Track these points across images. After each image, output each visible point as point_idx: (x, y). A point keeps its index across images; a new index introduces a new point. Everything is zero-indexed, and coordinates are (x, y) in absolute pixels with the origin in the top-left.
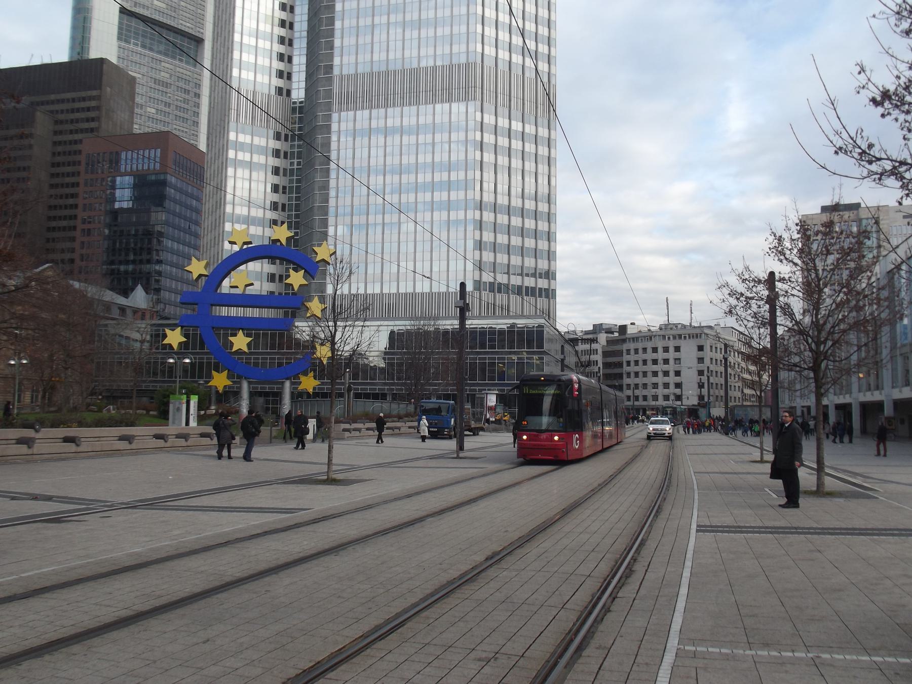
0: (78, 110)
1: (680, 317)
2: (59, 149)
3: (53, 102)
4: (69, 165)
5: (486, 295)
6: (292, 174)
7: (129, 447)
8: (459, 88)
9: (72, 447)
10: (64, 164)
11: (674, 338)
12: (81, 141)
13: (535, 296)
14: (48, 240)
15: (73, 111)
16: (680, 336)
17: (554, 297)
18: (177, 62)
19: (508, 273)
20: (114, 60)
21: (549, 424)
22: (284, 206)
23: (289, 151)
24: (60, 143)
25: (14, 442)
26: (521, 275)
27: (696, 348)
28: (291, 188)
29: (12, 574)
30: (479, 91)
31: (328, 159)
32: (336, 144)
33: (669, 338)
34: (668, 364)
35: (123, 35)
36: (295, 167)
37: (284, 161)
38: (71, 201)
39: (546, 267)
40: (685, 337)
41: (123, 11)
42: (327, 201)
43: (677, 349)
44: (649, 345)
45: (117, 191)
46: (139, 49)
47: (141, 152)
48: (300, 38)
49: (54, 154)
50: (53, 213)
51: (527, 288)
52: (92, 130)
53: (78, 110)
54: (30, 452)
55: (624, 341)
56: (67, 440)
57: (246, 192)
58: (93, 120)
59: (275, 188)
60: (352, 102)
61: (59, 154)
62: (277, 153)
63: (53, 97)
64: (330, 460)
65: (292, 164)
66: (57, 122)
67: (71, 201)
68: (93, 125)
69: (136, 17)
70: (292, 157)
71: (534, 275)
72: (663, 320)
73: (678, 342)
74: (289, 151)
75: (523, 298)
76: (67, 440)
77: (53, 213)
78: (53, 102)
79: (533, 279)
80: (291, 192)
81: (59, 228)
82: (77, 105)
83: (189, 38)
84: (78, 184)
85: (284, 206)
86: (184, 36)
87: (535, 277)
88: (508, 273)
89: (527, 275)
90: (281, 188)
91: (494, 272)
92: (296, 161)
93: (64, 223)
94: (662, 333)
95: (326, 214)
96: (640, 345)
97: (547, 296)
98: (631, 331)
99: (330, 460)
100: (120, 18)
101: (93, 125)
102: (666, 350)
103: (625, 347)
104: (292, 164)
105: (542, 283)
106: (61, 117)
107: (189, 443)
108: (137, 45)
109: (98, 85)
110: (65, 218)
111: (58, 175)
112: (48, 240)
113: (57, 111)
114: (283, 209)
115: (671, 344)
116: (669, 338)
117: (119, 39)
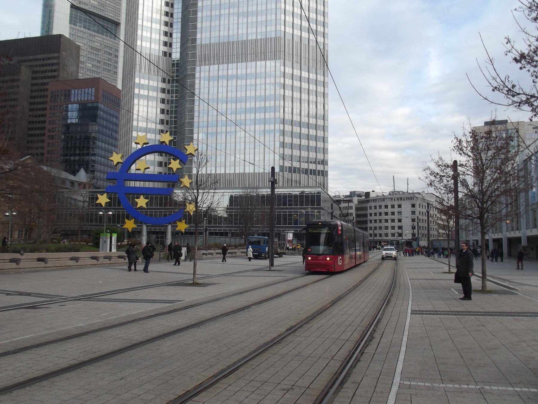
0: (46, 65)
1: (401, 187)
2: (35, 88)
3: (31, 60)
4: (41, 98)
5: (287, 174)
6: (172, 103)
7: (76, 264)
8: (271, 52)
9: (42, 264)
10: (38, 97)
11: (398, 199)
12: (48, 83)
13: (316, 175)
14: (28, 142)
15: (43, 65)
16: (401, 199)
17: (327, 175)
18: (105, 37)
19: (300, 161)
20: (67, 35)
21: (324, 251)
22: (167, 121)
23: (171, 89)
24: (35, 84)
25: (8, 261)
26: (308, 162)
27: (411, 206)
28: (172, 111)
29: (7, 339)
30: (282, 54)
31: (194, 94)
32: (198, 85)
33: (395, 200)
34: (394, 215)
35: (73, 21)
36: (174, 98)
37: (167, 95)
38: (42, 119)
39: (322, 158)
40: (404, 199)
41: (73, 6)
42: (193, 119)
43: (400, 206)
44: (383, 204)
45: (69, 113)
46: (82, 29)
47: (83, 90)
48: (177, 22)
49: (32, 91)
50: (31, 126)
51: (311, 170)
52: (54, 77)
53: (46, 65)
54: (18, 267)
55: (368, 201)
56: (39, 260)
57: (145, 113)
58: (55, 71)
59: (162, 111)
60: (208, 60)
61: (35, 91)
62: (163, 91)
63: (31, 57)
64: (195, 271)
65: (172, 97)
66: (33, 72)
67: (42, 119)
68: (55, 74)
69: (80, 10)
70: (172, 93)
71: (315, 163)
72: (391, 189)
73: (400, 202)
74: (171, 89)
75: (308, 176)
76: (39, 260)
77: (31, 126)
78: (31, 60)
79: (314, 165)
80: (172, 113)
81: (35, 135)
82: (46, 62)
83: (111, 22)
84: (46, 109)
85: (167, 121)
86: (109, 21)
87: (316, 164)
88: (300, 161)
89: (311, 162)
90: (166, 111)
91: (292, 160)
92: (174, 95)
93: (38, 132)
94: (391, 197)
95: (193, 126)
96: (377, 204)
97: (323, 175)
98: (372, 195)
99: (195, 271)
100: (71, 11)
101: (55, 74)
102: (393, 206)
103: (369, 205)
104: (172, 97)
105: (320, 167)
106: (36, 69)
107: (111, 262)
108: (81, 26)
109: (58, 50)
110: (38, 129)
111: (34, 103)
112: (28, 142)
113: (34, 66)
114: (167, 124)
115: (396, 203)
116: (395, 200)
117: (70, 23)
